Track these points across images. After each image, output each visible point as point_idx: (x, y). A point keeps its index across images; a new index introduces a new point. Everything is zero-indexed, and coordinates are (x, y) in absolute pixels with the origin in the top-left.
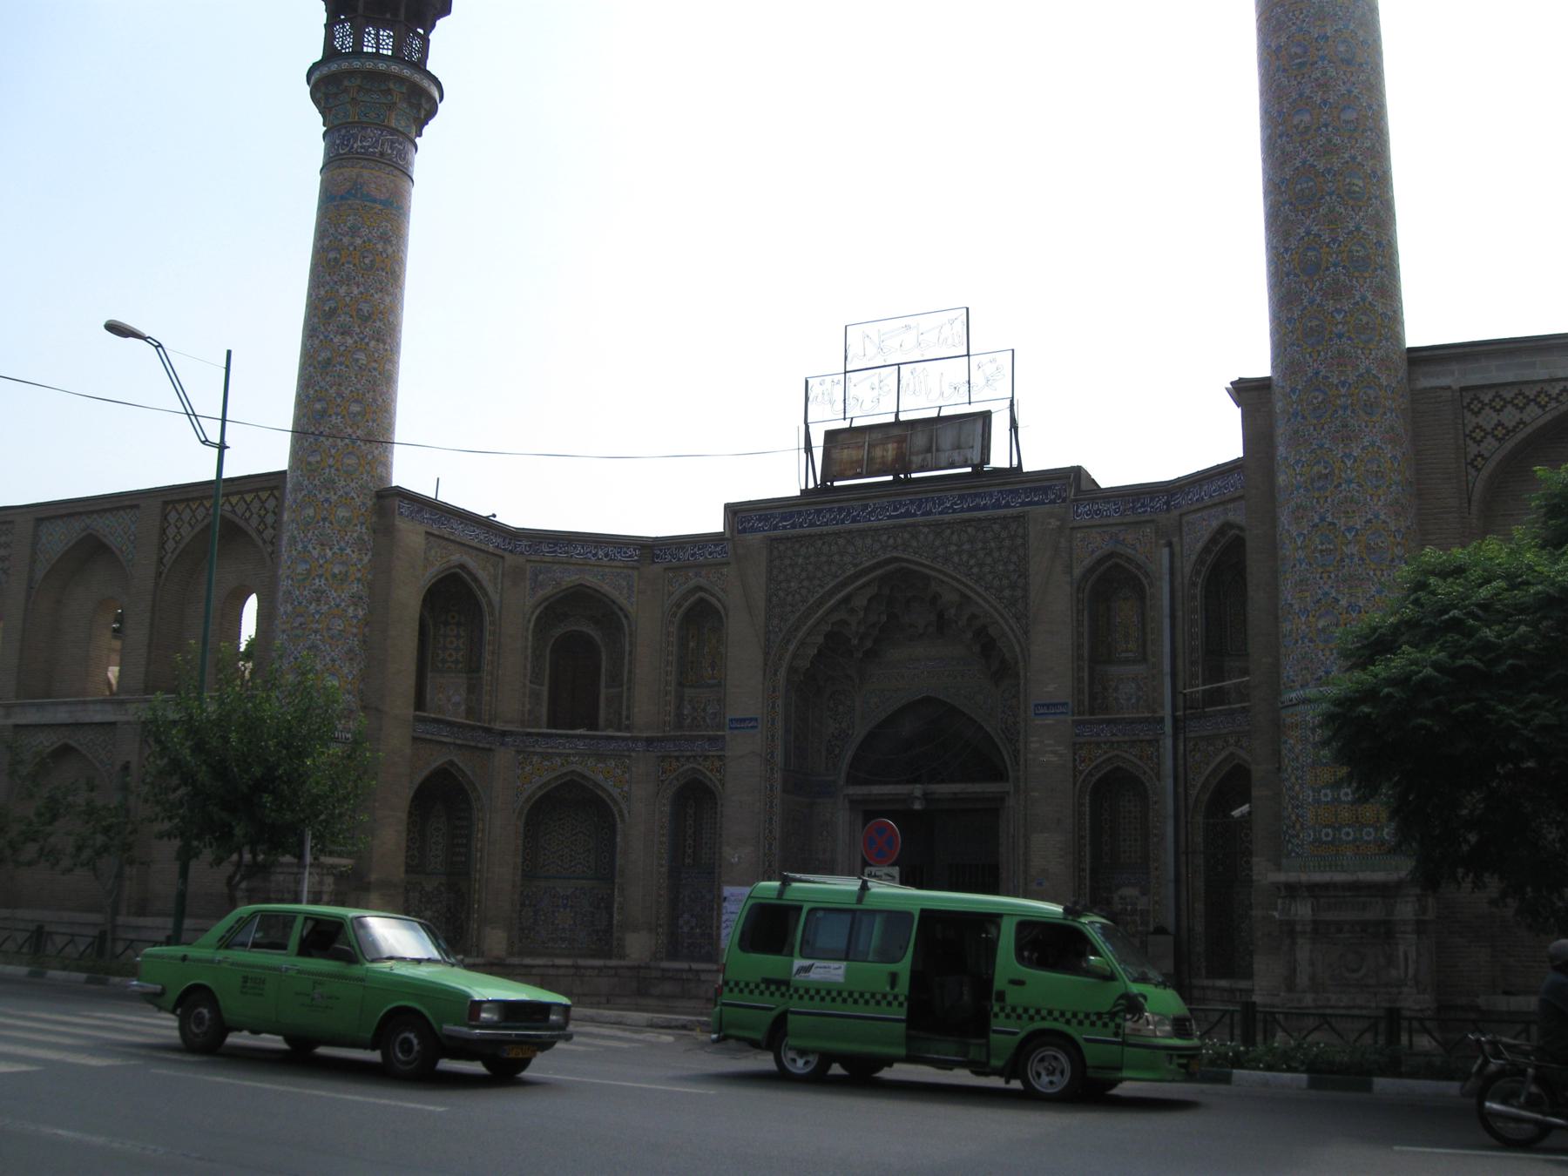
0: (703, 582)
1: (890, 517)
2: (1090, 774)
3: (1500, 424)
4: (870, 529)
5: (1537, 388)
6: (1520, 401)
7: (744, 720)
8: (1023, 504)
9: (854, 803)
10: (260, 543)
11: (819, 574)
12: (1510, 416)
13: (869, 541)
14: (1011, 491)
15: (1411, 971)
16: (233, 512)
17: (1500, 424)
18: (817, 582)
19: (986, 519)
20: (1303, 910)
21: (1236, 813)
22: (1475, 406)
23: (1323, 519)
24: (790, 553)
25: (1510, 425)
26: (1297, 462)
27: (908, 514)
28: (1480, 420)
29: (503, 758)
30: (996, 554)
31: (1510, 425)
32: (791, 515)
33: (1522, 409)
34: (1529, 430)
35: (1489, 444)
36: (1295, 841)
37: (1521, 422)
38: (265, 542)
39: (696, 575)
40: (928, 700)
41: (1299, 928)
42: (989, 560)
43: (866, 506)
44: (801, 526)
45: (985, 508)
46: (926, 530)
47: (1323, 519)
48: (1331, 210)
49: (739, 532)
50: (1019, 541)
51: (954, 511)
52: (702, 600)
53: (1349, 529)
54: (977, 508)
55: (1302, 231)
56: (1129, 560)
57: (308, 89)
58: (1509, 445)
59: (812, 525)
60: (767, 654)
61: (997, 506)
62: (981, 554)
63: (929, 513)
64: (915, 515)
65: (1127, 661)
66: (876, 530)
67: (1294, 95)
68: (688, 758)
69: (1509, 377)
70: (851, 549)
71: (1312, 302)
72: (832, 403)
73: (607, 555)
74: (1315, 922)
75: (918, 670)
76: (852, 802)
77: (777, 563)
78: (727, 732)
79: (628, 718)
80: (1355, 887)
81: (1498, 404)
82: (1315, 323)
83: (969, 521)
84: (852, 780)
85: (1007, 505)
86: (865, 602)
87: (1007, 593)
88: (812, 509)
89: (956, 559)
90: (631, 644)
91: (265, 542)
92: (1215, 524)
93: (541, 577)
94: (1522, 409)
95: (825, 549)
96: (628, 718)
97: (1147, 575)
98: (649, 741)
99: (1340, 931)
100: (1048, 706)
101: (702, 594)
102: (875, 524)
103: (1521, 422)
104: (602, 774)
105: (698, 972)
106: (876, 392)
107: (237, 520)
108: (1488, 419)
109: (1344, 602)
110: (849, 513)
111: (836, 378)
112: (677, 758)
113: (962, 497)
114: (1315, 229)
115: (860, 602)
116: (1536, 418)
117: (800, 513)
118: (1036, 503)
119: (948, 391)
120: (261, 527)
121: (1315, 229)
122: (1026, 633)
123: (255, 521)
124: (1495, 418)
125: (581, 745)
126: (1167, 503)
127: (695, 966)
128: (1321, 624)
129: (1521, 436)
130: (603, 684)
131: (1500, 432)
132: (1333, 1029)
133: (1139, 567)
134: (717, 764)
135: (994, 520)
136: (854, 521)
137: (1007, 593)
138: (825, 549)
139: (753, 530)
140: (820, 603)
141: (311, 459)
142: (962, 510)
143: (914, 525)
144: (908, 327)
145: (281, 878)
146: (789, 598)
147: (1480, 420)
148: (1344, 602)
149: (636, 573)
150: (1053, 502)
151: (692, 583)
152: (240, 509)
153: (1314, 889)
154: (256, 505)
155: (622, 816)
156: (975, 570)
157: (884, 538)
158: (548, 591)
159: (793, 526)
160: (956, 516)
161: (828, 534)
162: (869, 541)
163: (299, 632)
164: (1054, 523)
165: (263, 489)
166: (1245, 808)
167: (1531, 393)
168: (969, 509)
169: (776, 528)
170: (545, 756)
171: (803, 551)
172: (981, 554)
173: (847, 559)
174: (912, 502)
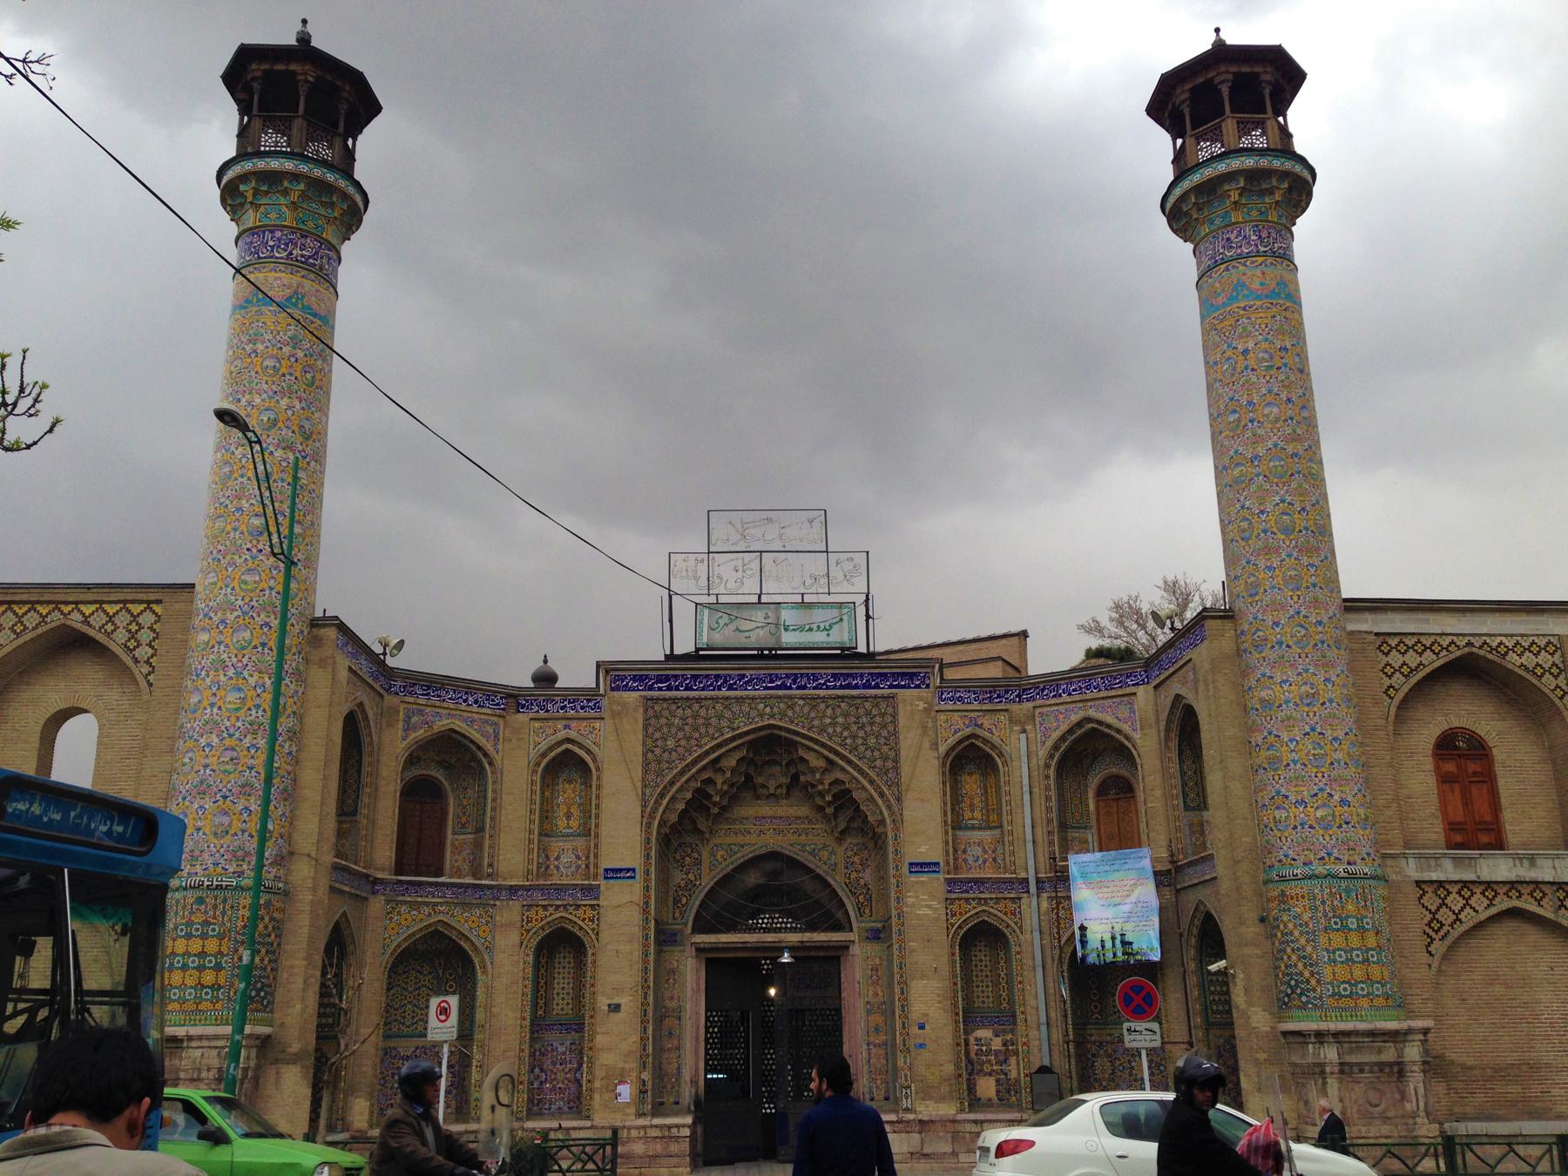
0: (573, 734)
1: (766, 688)
2: (960, 927)
3: (1404, 664)
4: (748, 697)
5: (1432, 639)
6: (1419, 648)
7: (621, 870)
8: (891, 687)
9: (700, 950)
10: (130, 663)
11: (697, 735)
12: (1412, 659)
13: (746, 708)
14: (880, 675)
15: (1422, 1104)
16: (86, 622)
17: (1404, 664)
18: (693, 742)
19: (858, 697)
20: (1330, 1053)
21: (1213, 968)
22: (1385, 648)
23: (1313, 729)
24: (666, 713)
25: (1413, 666)
26: (1284, 682)
27: (784, 687)
28: (1389, 659)
29: (377, 904)
30: (868, 729)
31: (1413, 666)
32: (667, 678)
33: (1421, 654)
34: (1428, 670)
35: (1398, 679)
36: (1312, 994)
37: (1421, 663)
38: (136, 661)
39: (566, 727)
40: (774, 856)
41: (1328, 1069)
42: (861, 734)
43: (744, 676)
44: (677, 689)
45: (856, 687)
46: (801, 702)
47: (1313, 729)
48: (1300, 486)
49: (613, 689)
50: (888, 719)
51: (828, 688)
52: (567, 750)
53: (1291, 740)
54: (849, 687)
55: (1277, 499)
56: (985, 741)
57: (218, 192)
58: (1413, 681)
59: (688, 688)
60: (644, 806)
61: (867, 686)
62: (854, 728)
63: (804, 687)
64: (790, 688)
65: (973, 828)
66: (753, 698)
67: (1264, 390)
68: (558, 907)
69: (1411, 628)
70: (728, 714)
71: (1289, 556)
72: (696, 578)
73: (476, 702)
74: (1341, 1064)
75: (769, 827)
76: (699, 950)
77: (653, 721)
78: (602, 882)
79: (491, 865)
80: (1372, 1034)
81: (1402, 648)
82: (1293, 573)
83: (843, 697)
84: (701, 926)
85: (877, 687)
86: (734, 763)
87: (878, 763)
88: (689, 673)
89: (830, 730)
90: (494, 791)
91: (136, 661)
92: (1074, 718)
93: (414, 719)
94: (1421, 654)
95: (703, 712)
96: (491, 865)
97: (1001, 755)
98: (513, 890)
99: (1362, 1071)
100: (921, 865)
101: (570, 746)
102: (752, 693)
103: (1421, 663)
104: (465, 922)
105: (568, 1129)
106: (740, 574)
107: (91, 633)
108: (1395, 659)
109: (1336, 797)
110: (725, 681)
111: (700, 557)
112: (545, 907)
113: (834, 675)
114: (1289, 499)
115: (732, 762)
116: (1432, 662)
117: (676, 676)
118: (903, 687)
119: (809, 582)
120: (132, 644)
121: (1289, 499)
122: (899, 799)
123: (121, 635)
124: (1401, 659)
125: (449, 893)
126: (1019, 696)
127: (565, 1124)
128: (1319, 813)
129: (1421, 675)
130: (450, 831)
131: (1405, 670)
132: (1395, 1155)
133: (994, 747)
134: (590, 913)
135: (866, 698)
136: (730, 688)
137: (878, 763)
138: (703, 712)
139: (627, 688)
140: (694, 762)
141: (248, 578)
142: (835, 687)
143: (790, 698)
144: (770, 520)
145: (198, 1053)
146: (666, 755)
147: (1389, 659)
148: (1336, 797)
149: (501, 721)
150: (918, 687)
151: (562, 734)
152: (98, 620)
153: (1339, 1036)
154: (123, 619)
155: (484, 967)
156: (849, 741)
157: (761, 706)
158: (420, 734)
159: (669, 688)
160: (830, 692)
161: (706, 699)
162: (746, 708)
163: (229, 767)
164: (922, 706)
165: (66, 603)
166: (1222, 964)
167: (1445, 642)
168: (841, 687)
169: (651, 688)
170: (414, 905)
171: (680, 712)
172: (854, 728)
173: (725, 723)
174: (787, 676)
